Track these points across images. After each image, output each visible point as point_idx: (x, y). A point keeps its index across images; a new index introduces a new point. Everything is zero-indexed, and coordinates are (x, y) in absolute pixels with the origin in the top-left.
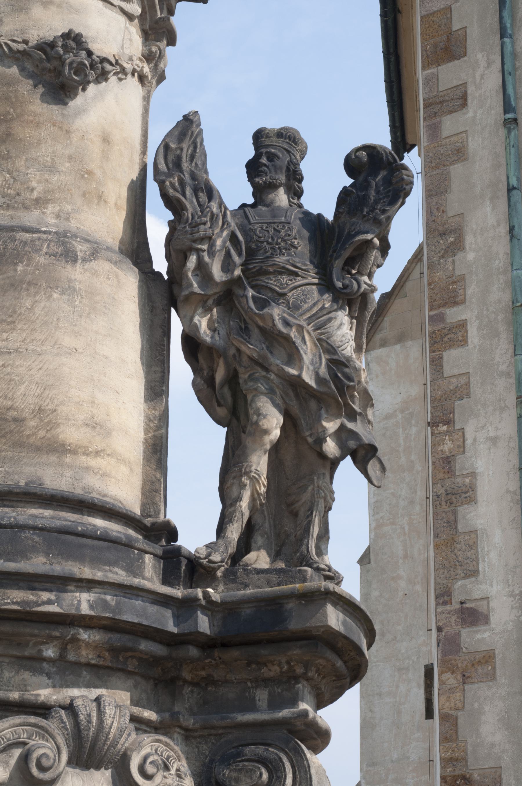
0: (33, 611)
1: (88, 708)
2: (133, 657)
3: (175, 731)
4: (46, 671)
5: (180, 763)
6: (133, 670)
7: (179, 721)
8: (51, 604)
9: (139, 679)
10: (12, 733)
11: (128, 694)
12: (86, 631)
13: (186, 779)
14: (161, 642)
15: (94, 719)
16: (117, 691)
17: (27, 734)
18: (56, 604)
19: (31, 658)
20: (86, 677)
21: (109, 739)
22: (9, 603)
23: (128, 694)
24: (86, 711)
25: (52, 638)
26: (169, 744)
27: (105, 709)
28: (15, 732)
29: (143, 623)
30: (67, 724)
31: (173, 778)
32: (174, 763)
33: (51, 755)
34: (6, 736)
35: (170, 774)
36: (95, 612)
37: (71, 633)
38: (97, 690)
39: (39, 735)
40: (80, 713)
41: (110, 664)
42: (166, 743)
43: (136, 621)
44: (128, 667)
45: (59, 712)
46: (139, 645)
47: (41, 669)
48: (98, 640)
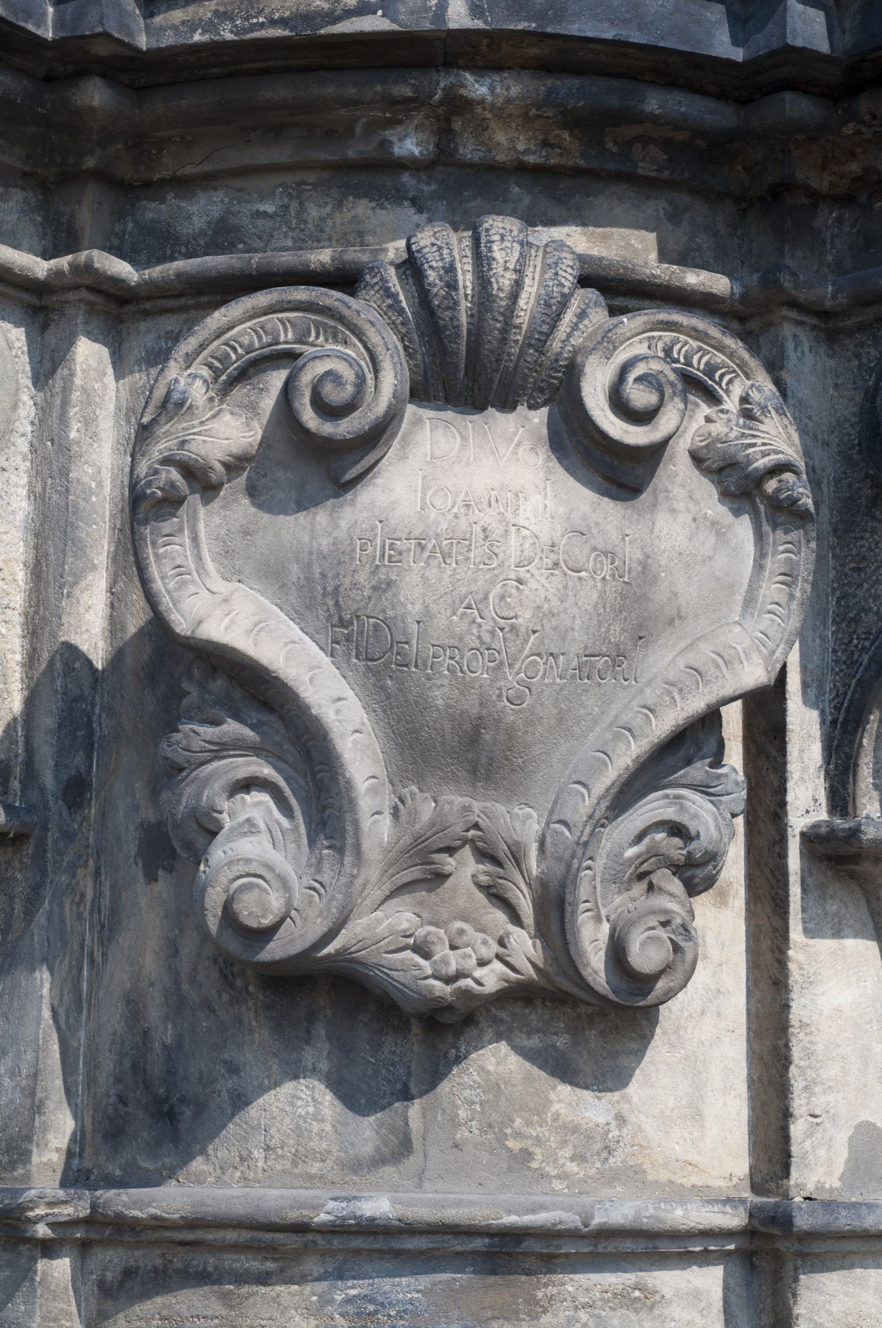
0: (321, 36)
1: (445, 251)
2: (645, 140)
3: (784, 318)
4: (411, 194)
5: (749, 383)
6: (654, 174)
7: (781, 289)
8: (367, 14)
9: (684, 199)
10: (255, 331)
11: (652, 237)
12: (483, 76)
13: (766, 421)
14: (721, 96)
15: (466, 279)
16: (614, 230)
17: (294, 332)
18: (380, 12)
19: (367, 166)
20: (520, 200)
21: (519, 327)
22: (262, 25)
23: (653, 236)
24: (443, 259)
25: (408, 105)
26: (706, 334)
27: (490, 250)
28: (262, 328)
29: (631, 40)
30: (402, 297)
31: (729, 421)
32: (730, 382)
33: (348, 375)
34: (240, 339)
35: (722, 411)
36: (486, 22)
37: (442, 85)
38: (553, 229)
39: (325, 331)
40: (426, 266)
41: (582, 163)
42: (695, 330)
43: (608, 35)
44: (637, 166)
45: (379, 272)
46: (642, 101)
47: (397, 190)
48: (517, 98)
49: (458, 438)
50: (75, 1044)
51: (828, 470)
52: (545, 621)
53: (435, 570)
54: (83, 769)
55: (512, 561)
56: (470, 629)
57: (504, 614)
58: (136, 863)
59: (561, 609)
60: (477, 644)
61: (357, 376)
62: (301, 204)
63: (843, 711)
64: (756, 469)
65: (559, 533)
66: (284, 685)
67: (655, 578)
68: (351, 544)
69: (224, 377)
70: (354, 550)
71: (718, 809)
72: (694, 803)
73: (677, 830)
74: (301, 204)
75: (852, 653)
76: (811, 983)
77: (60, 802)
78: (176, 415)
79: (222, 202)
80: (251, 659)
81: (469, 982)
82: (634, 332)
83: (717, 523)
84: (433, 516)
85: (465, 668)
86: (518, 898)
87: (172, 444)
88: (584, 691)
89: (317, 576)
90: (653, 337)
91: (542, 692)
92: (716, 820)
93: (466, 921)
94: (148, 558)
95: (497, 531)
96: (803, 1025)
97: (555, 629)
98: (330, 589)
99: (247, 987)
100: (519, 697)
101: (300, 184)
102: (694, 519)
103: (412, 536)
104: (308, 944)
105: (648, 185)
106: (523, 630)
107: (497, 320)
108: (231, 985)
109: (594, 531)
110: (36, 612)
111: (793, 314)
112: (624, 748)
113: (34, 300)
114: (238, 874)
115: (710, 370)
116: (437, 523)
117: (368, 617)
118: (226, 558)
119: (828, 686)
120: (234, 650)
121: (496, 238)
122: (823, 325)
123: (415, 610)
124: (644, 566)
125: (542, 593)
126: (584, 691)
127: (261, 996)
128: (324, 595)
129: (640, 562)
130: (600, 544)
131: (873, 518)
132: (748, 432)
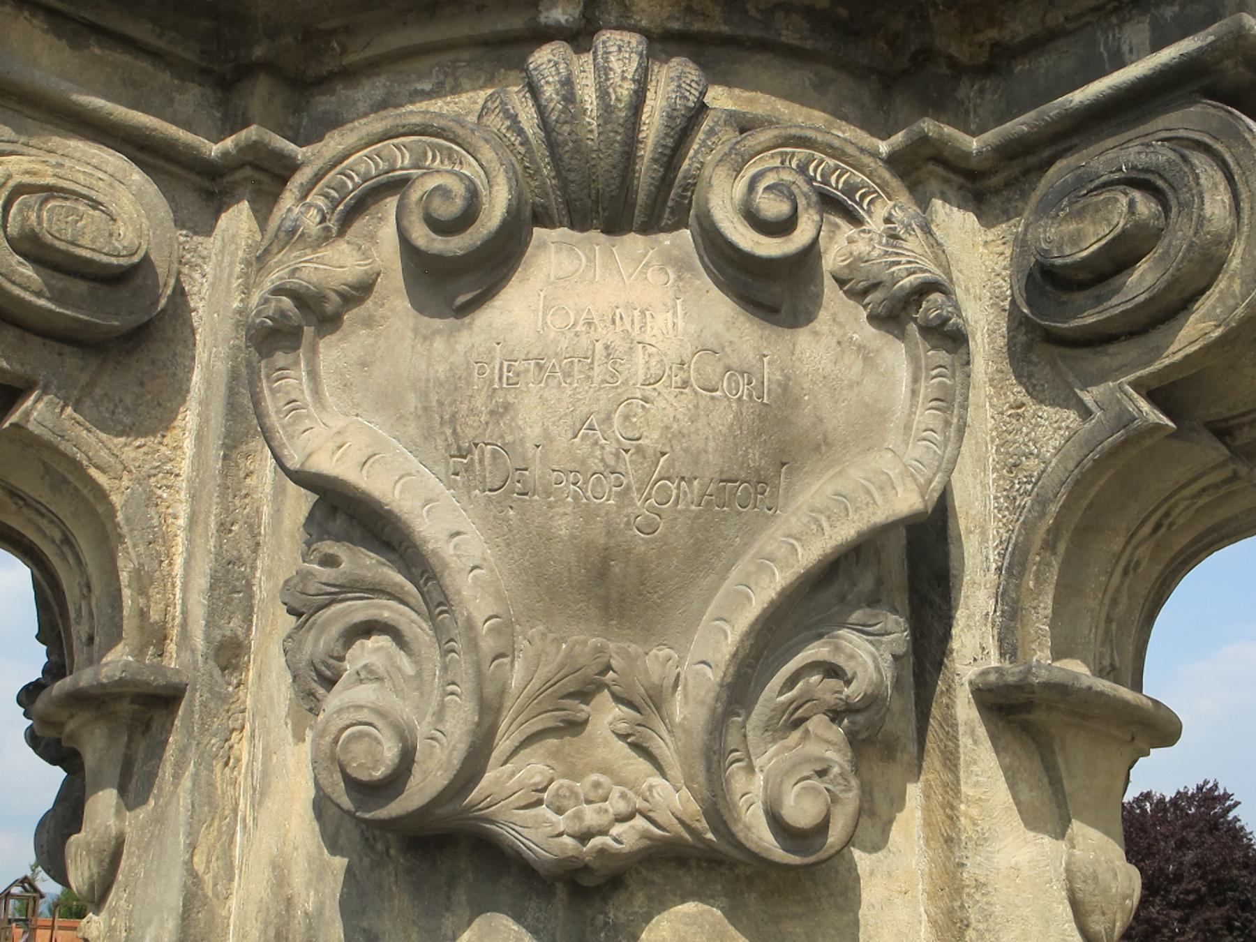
1: (562, 66)
3: (931, 173)
5: (891, 204)
6: (797, 43)
9: (830, 72)
27: (607, 61)
31: (871, 239)
41: (725, 29)
49: (584, 260)
50: (224, 913)
51: (982, 323)
52: (674, 442)
53: (555, 391)
54: (240, 632)
55: (640, 381)
56: (593, 452)
57: (630, 435)
58: (286, 724)
59: (693, 430)
60: (601, 467)
61: (468, 189)
62: (456, 80)
63: (1007, 556)
64: (902, 287)
65: (689, 351)
66: (398, 519)
67: (797, 402)
68: (468, 367)
69: (341, 207)
70: (470, 375)
71: (877, 649)
72: (850, 642)
73: (832, 671)
74: (456, 80)
75: (1015, 498)
76: (986, 840)
77: (212, 663)
78: (287, 243)
79: (384, 85)
80: (363, 492)
81: (607, 840)
82: (765, 145)
83: (865, 347)
84: (552, 336)
85: (589, 494)
86: (660, 747)
87: (284, 273)
88: (722, 519)
89: (434, 403)
90: (786, 153)
91: (675, 519)
92: (875, 660)
93: (604, 773)
94: (262, 392)
95: (621, 349)
96: (979, 885)
97: (686, 450)
98: (447, 417)
99: (387, 850)
100: (649, 525)
101: (454, 62)
102: (839, 343)
103: (531, 356)
104: (426, 799)
105: (794, 54)
106: (650, 452)
107: (617, 132)
108: (372, 848)
109: (728, 350)
110: (197, 476)
111: (940, 170)
112: (768, 580)
113: (206, 184)
114: (348, 722)
115: (850, 190)
116: (556, 342)
117: (486, 444)
118: (344, 391)
119: (992, 533)
120: (344, 483)
121: (614, 49)
122: (969, 185)
123: (533, 433)
124: (785, 388)
125: (670, 412)
126: (722, 519)
127: (401, 860)
128: (442, 424)
129: (779, 384)
130: (734, 362)
131: (1030, 362)
132: (891, 250)
